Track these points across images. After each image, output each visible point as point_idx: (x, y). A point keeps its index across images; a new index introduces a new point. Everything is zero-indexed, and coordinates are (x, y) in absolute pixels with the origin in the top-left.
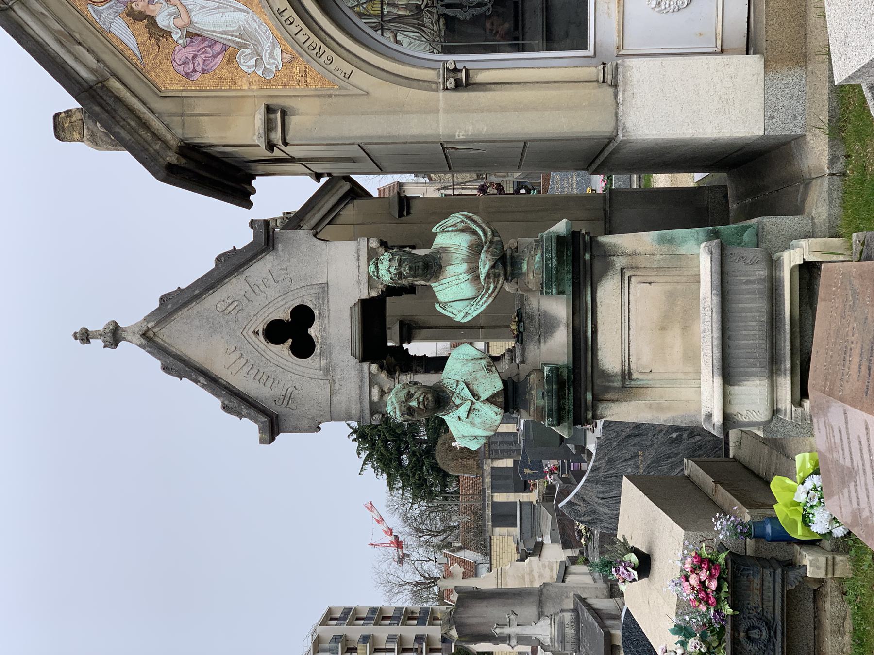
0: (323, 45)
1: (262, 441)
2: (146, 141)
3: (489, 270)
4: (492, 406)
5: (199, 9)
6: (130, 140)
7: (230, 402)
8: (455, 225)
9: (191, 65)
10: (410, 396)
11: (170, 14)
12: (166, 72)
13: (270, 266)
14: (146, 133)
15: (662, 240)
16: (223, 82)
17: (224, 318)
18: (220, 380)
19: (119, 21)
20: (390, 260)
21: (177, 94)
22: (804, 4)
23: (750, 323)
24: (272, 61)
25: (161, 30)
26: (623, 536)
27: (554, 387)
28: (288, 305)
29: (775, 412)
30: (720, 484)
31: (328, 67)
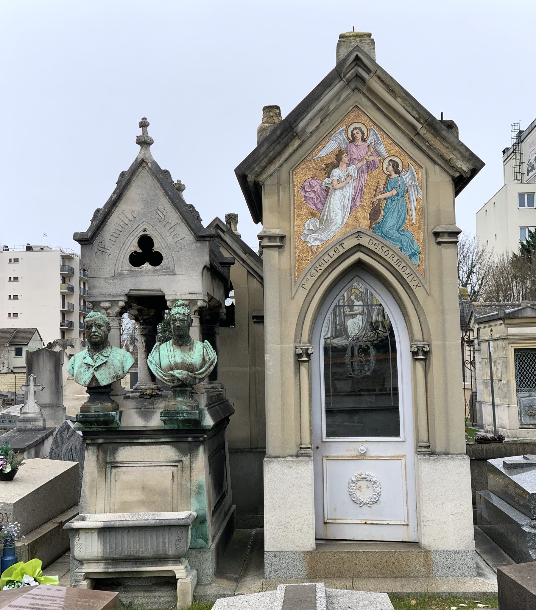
0: (322, 271)
1: (75, 234)
2: (260, 162)
3: (176, 377)
4: (90, 379)
5: (343, 195)
6: (260, 153)
7: (101, 214)
8: (207, 354)
9: (309, 190)
10: (99, 326)
11: (340, 177)
12: (305, 175)
13: (187, 238)
14: (265, 162)
15: (200, 487)
16: (299, 209)
17: (154, 210)
18: (115, 208)
19: (336, 146)
20: (184, 314)
21: (291, 181)
22: (347, 577)
23: (138, 545)
24: (312, 240)
25: (331, 171)
26: (24, 463)
27: (102, 419)
28: (162, 250)
29: (81, 562)
30: (59, 526)
31: (309, 274)
